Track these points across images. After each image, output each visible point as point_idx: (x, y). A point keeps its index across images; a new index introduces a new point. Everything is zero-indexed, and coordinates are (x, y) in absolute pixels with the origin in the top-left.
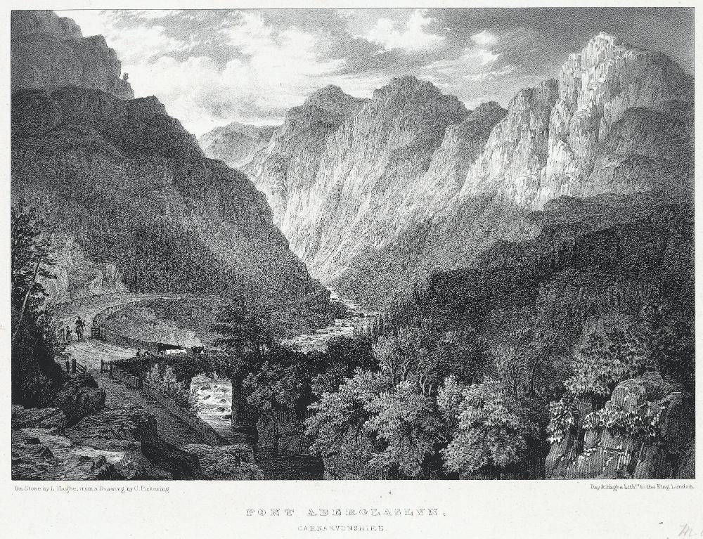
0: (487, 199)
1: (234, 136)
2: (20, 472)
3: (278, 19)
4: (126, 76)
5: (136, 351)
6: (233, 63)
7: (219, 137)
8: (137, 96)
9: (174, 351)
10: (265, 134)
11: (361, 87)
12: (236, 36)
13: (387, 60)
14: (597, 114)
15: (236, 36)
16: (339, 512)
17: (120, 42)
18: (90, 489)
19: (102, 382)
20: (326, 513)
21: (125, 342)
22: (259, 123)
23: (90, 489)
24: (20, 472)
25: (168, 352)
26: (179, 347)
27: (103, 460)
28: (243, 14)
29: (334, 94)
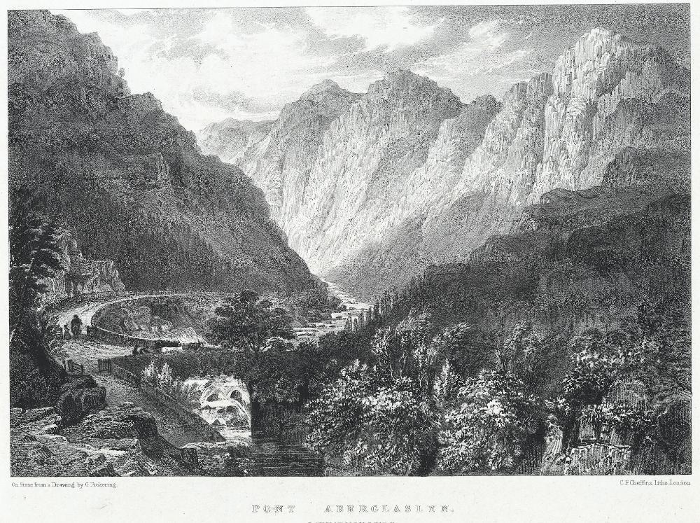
0: (480, 196)
1: (236, 132)
2: (19, 467)
3: (250, 18)
4: (122, 73)
5: (132, 348)
6: (211, 60)
7: (215, 134)
8: (133, 92)
9: (170, 349)
10: (264, 128)
11: (356, 83)
12: (208, 34)
13: (378, 58)
14: (592, 109)
15: (208, 34)
16: (374, 508)
17: (113, 38)
18: (44, 485)
19: (99, 380)
20: (363, 508)
21: (123, 342)
22: (258, 118)
23: (44, 485)
24: (19, 467)
25: (164, 349)
26: (176, 344)
27: (102, 458)
28: (215, 11)
29: (336, 93)
